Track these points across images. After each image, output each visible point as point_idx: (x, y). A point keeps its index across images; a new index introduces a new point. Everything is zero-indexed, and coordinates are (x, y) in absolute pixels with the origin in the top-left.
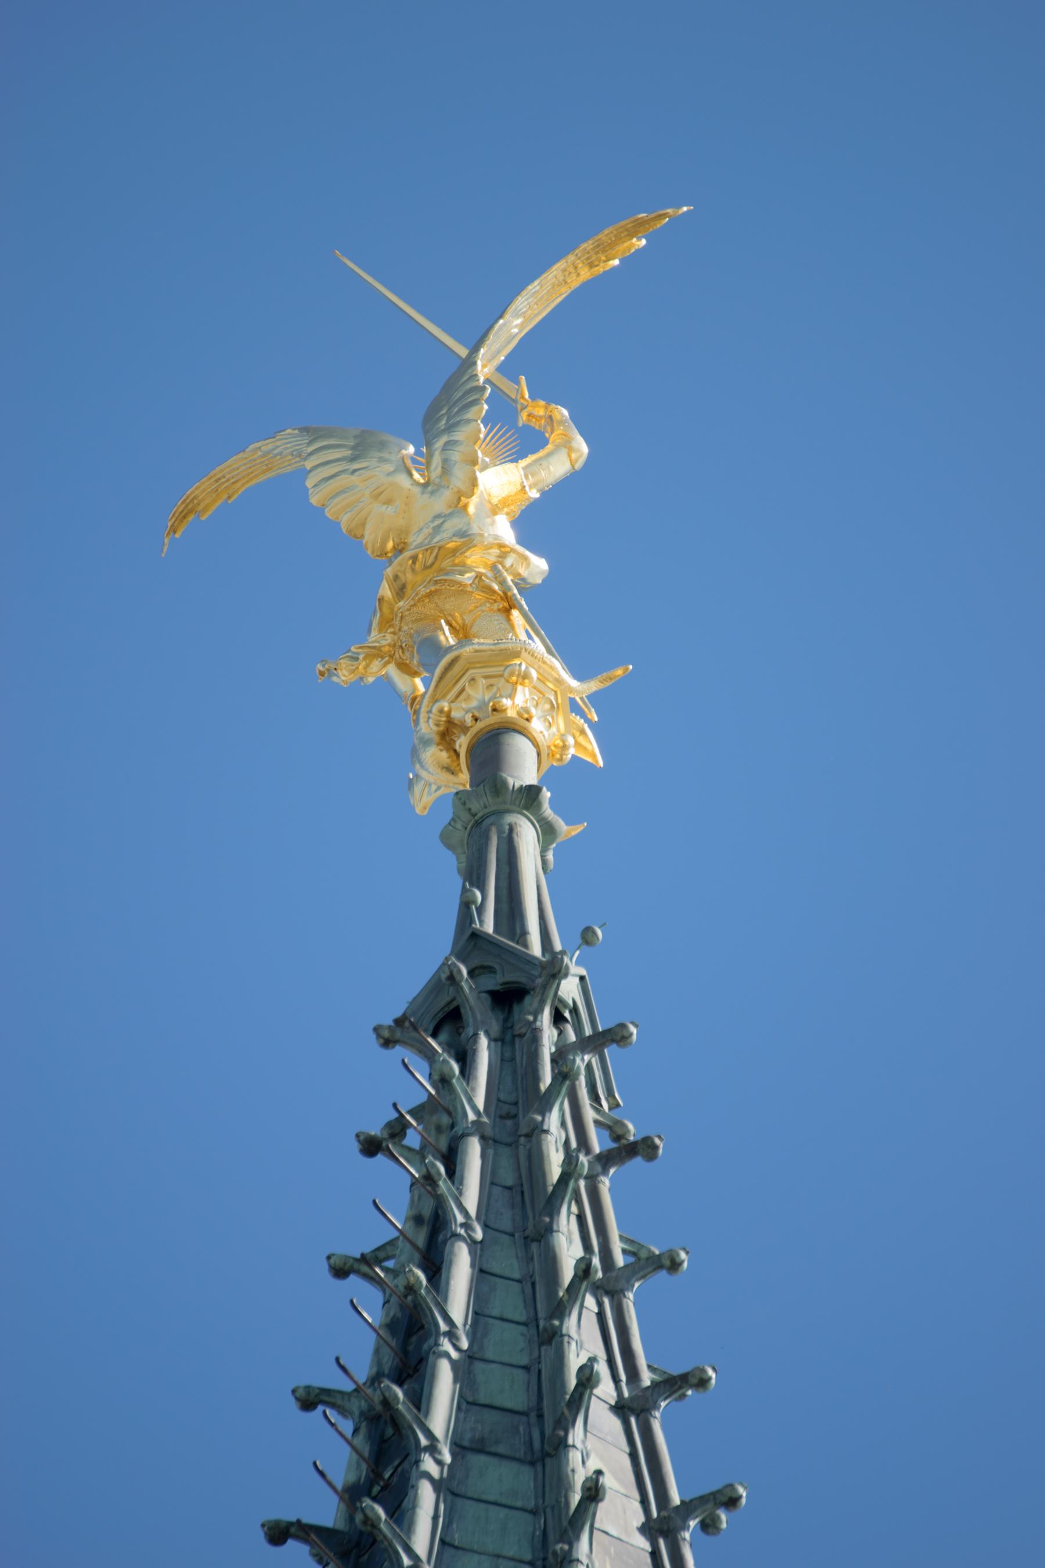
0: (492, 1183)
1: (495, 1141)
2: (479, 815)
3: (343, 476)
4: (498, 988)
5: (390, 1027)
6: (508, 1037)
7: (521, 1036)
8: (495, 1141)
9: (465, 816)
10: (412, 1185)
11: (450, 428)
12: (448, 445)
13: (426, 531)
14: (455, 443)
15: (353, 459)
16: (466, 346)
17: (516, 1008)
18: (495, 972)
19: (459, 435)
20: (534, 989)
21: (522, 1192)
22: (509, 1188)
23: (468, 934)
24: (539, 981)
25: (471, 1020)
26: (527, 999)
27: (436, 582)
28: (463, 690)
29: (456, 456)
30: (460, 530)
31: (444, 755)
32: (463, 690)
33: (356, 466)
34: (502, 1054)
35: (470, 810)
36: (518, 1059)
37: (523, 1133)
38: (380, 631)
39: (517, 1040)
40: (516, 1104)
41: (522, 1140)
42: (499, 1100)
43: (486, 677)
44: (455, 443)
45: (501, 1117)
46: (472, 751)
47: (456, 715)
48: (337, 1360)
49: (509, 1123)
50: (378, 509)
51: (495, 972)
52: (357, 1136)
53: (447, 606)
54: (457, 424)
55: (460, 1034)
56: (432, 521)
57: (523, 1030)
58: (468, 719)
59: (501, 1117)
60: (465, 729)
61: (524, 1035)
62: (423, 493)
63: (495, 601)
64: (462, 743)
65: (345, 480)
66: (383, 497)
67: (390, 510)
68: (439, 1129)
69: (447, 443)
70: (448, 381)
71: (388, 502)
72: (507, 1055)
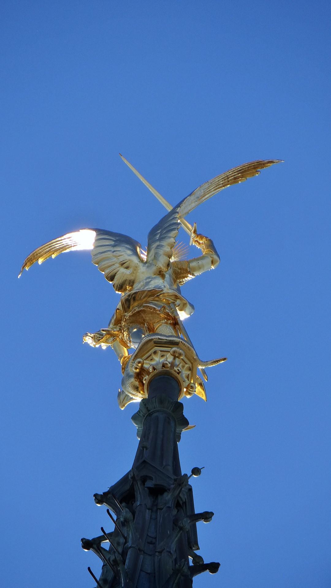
0: (141, 570)
1: (144, 553)
2: (151, 411)
3: (109, 253)
4: (153, 486)
5: (101, 495)
6: (155, 509)
7: (161, 509)
8: (144, 553)
9: (144, 411)
10: (103, 566)
11: (161, 239)
12: (158, 247)
13: (142, 283)
14: (162, 246)
15: (114, 246)
16: (171, 204)
17: (160, 498)
18: (152, 480)
19: (164, 243)
20: (169, 490)
21: (155, 576)
22: (149, 574)
23: (141, 461)
24: (172, 486)
25: (139, 498)
26: (165, 494)
27: (144, 307)
28: (151, 355)
29: (161, 252)
30: (158, 285)
31: (137, 383)
32: (151, 355)
33: (116, 249)
34: (151, 516)
35: (147, 408)
36: (158, 519)
37: (157, 551)
38: (115, 325)
39: (159, 511)
40: (155, 538)
41: (157, 554)
42: (147, 535)
43: (161, 351)
44: (162, 246)
45: (148, 543)
46: (150, 383)
47: (146, 366)
48: (89, 569)
49: (151, 546)
50: (122, 270)
51: (152, 480)
52: (82, 540)
53: (147, 319)
54: (164, 238)
55: (133, 504)
56: (146, 279)
57: (162, 507)
58: (151, 370)
59: (148, 543)
60: (148, 373)
61: (162, 509)
62: (143, 266)
63: (169, 319)
64: (146, 379)
65: (109, 254)
66: (125, 265)
67: (128, 272)
68: (118, 544)
69: (158, 246)
70: (162, 219)
71: (127, 268)
72: (153, 517)
